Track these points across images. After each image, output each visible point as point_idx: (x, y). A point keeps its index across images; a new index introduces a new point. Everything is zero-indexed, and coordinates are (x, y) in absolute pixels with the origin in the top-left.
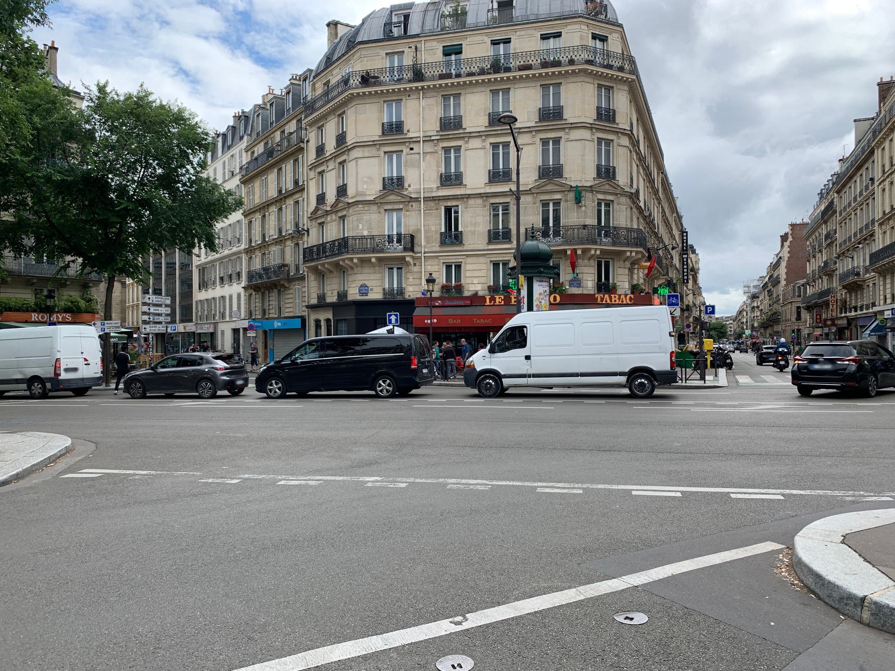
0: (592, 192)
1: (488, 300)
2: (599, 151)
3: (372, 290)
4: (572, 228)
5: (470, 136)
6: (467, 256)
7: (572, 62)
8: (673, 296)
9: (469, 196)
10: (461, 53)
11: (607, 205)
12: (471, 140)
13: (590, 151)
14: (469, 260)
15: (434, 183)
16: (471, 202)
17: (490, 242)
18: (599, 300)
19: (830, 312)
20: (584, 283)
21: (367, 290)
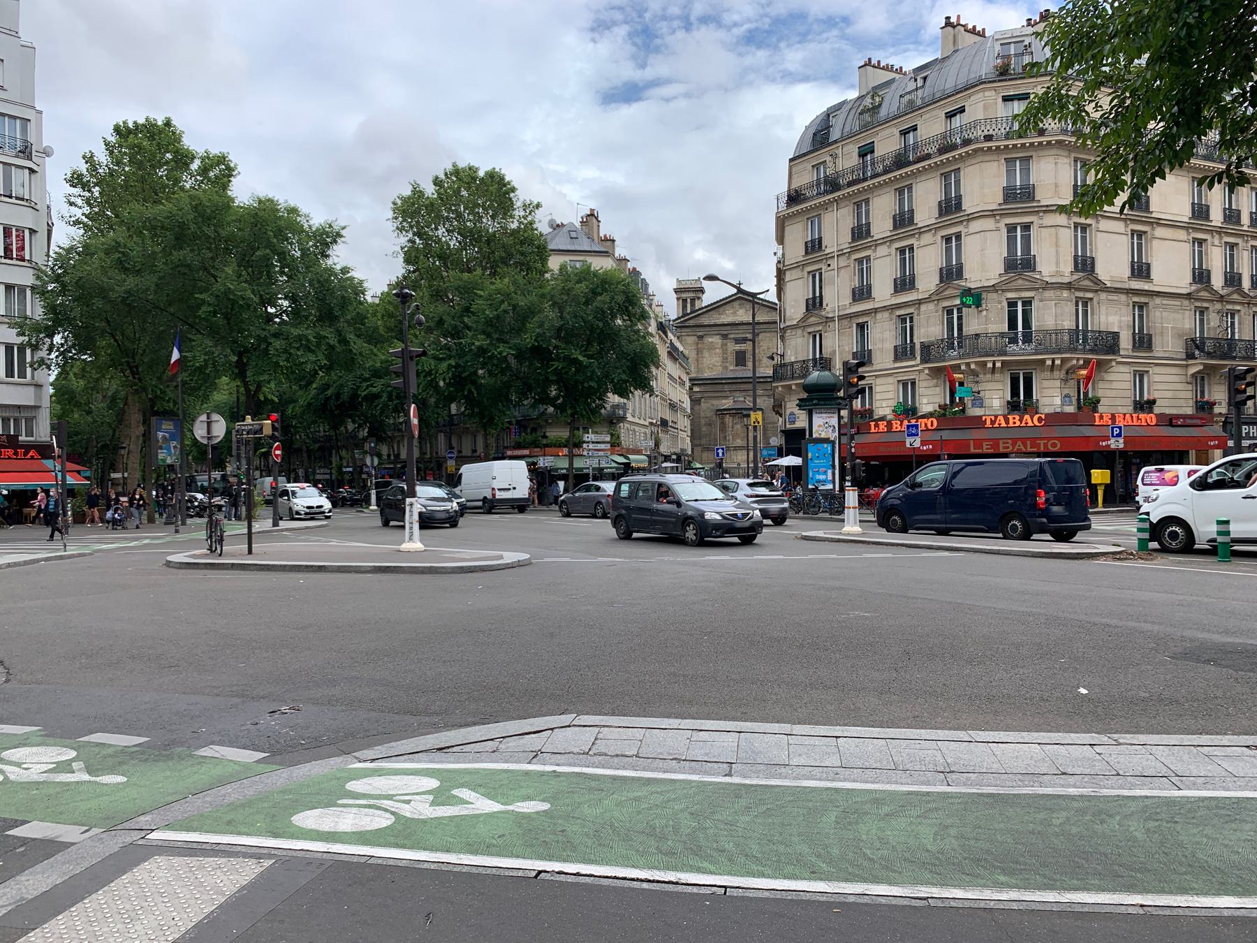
0: (1070, 289)
2: (1076, 237)
4: (1047, 333)
6: (876, 376)
7: (967, 142)
9: (876, 311)
10: (873, 152)
11: (1085, 304)
12: (879, 248)
13: (1067, 236)
14: (879, 381)
15: (847, 299)
16: (879, 316)
18: (988, 422)
20: (987, 402)
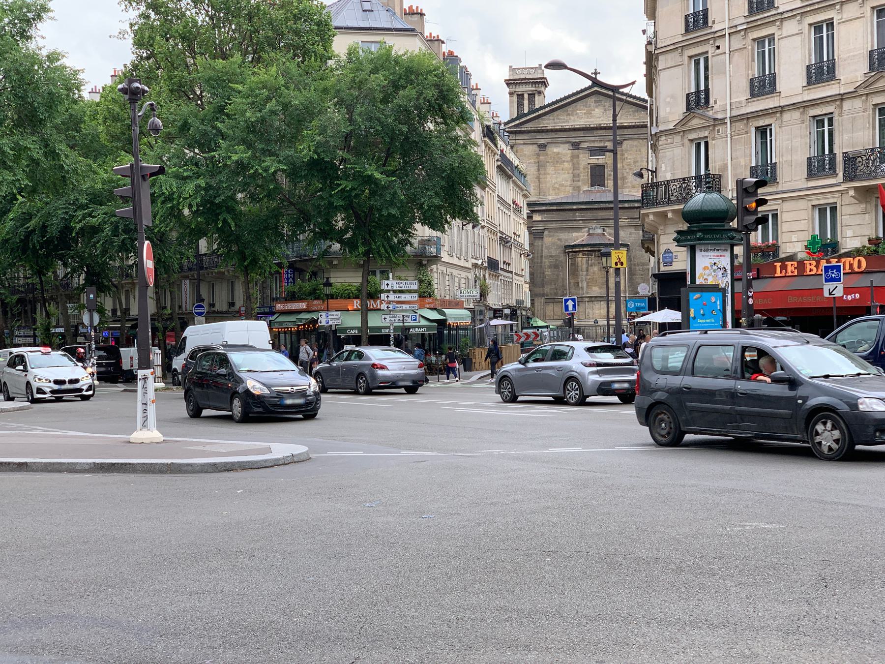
1: (778, 269)
3: (676, 257)
5: (783, 18)
6: (783, 200)
8: (832, 268)
14: (787, 206)
15: (743, 94)
16: (787, 116)
17: (811, 175)
19: (284, 284)
21: (671, 257)
